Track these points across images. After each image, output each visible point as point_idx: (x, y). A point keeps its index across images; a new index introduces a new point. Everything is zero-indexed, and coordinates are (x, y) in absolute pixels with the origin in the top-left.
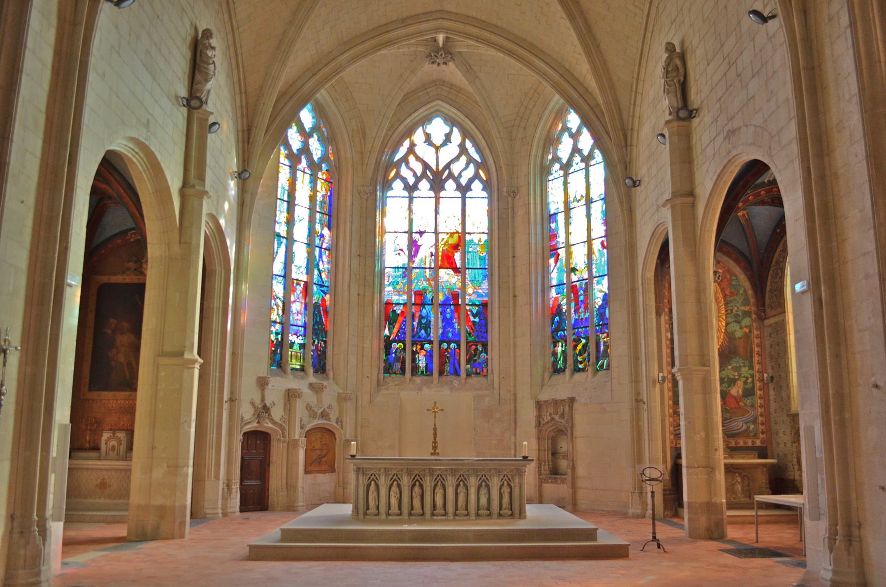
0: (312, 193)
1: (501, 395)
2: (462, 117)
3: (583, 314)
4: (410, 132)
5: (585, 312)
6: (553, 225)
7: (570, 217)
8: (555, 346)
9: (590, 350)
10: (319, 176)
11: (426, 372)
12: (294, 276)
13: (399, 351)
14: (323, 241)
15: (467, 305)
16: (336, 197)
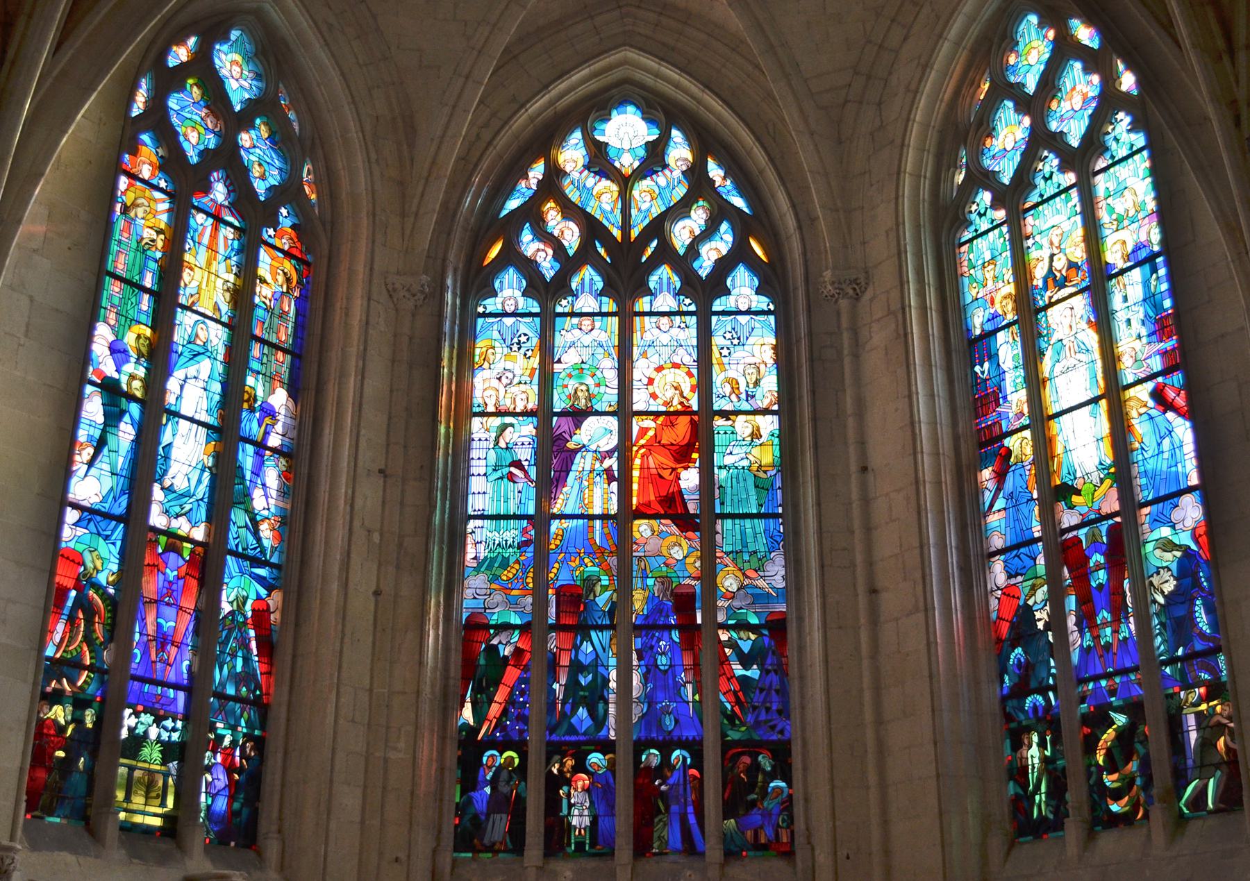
2: (695, 89)
3: (1108, 631)
7: (1040, 335)
8: (1018, 744)
9: (1152, 746)
12: (157, 519)
13: (504, 775)
16: (320, 303)
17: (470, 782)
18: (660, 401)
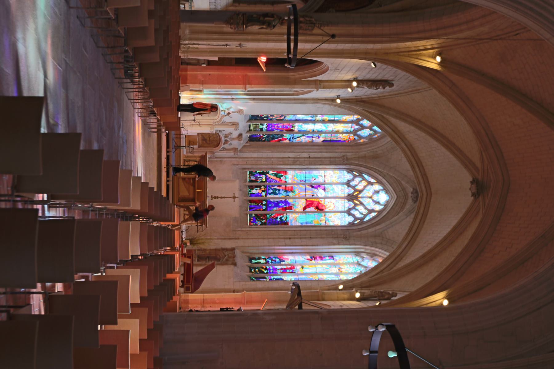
1: (238, 232)
2: (388, 210)
4: (379, 182)
5: (281, 272)
6: (327, 258)
11: (250, 193)
17: (260, 173)
18: (327, 204)
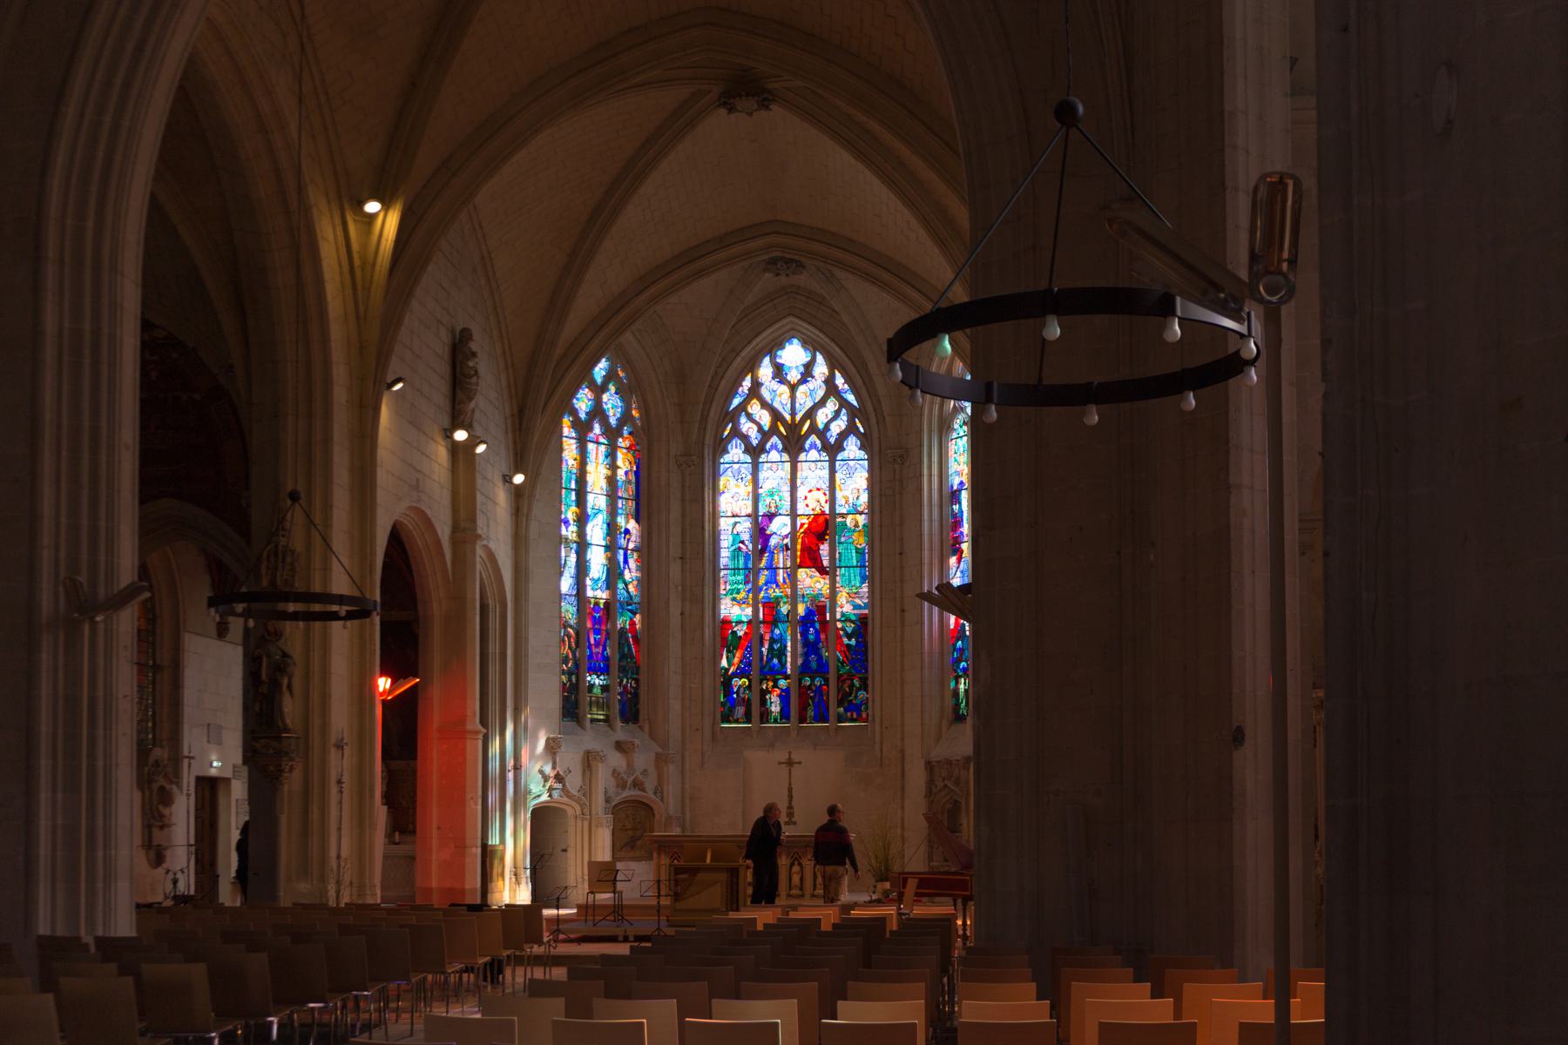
0: (609, 473)
4: (752, 366)
10: (619, 444)
11: (781, 719)
13: (742, 689)
14: (629, 540)
15: (839, 620)
